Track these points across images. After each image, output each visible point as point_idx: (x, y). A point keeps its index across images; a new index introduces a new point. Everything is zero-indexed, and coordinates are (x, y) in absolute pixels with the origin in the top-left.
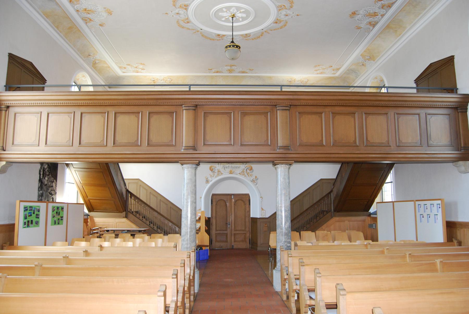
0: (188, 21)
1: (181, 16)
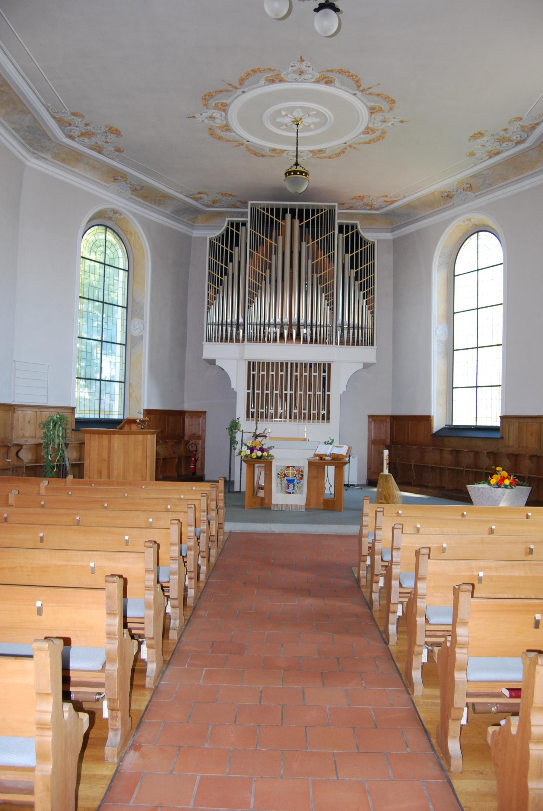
0: (227, 128)
1: (216, 121)
